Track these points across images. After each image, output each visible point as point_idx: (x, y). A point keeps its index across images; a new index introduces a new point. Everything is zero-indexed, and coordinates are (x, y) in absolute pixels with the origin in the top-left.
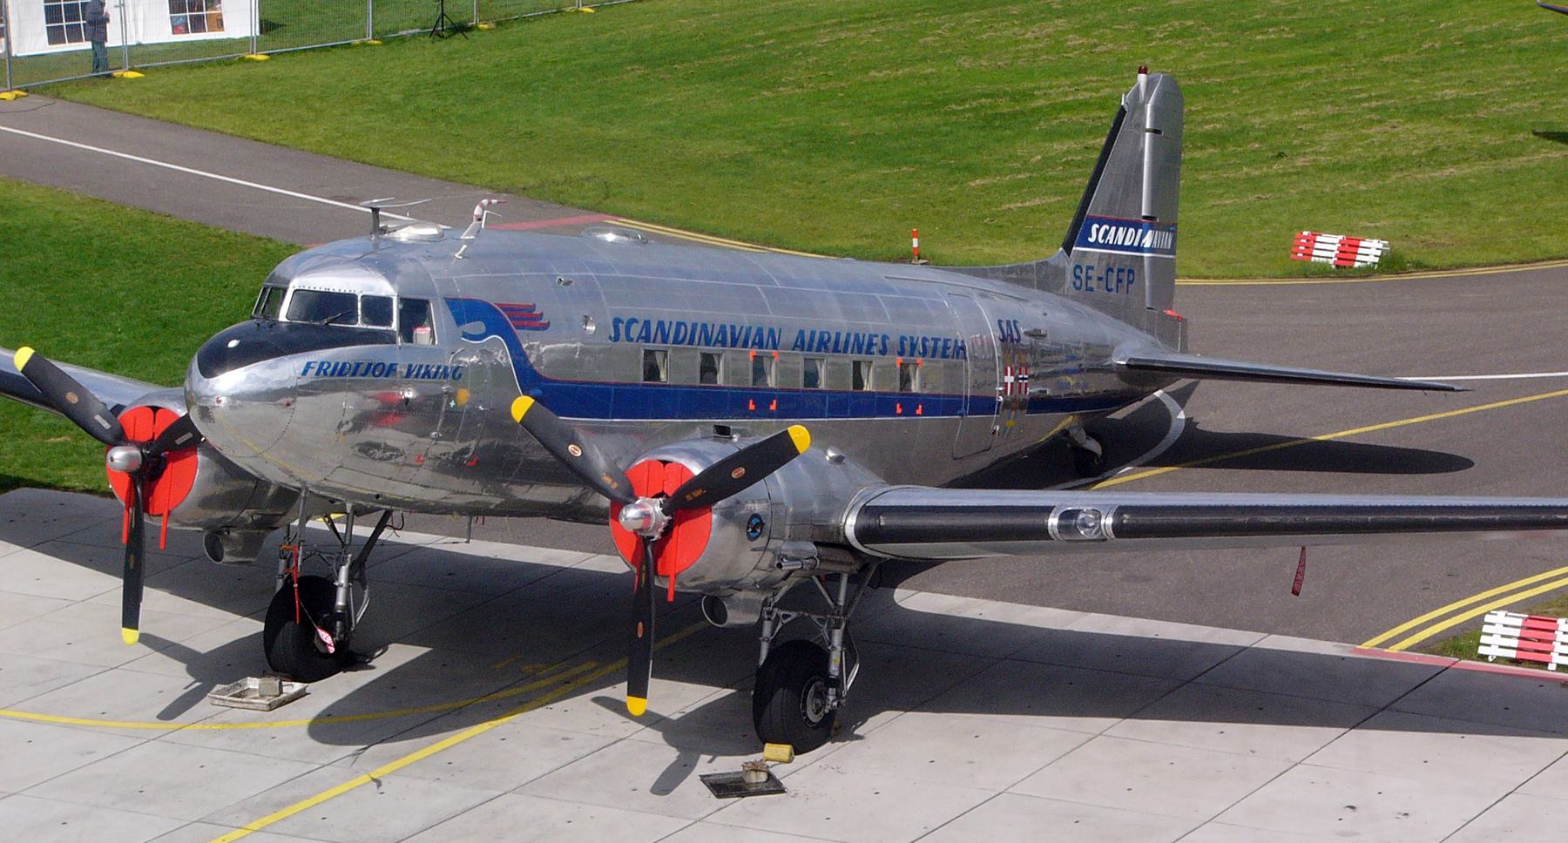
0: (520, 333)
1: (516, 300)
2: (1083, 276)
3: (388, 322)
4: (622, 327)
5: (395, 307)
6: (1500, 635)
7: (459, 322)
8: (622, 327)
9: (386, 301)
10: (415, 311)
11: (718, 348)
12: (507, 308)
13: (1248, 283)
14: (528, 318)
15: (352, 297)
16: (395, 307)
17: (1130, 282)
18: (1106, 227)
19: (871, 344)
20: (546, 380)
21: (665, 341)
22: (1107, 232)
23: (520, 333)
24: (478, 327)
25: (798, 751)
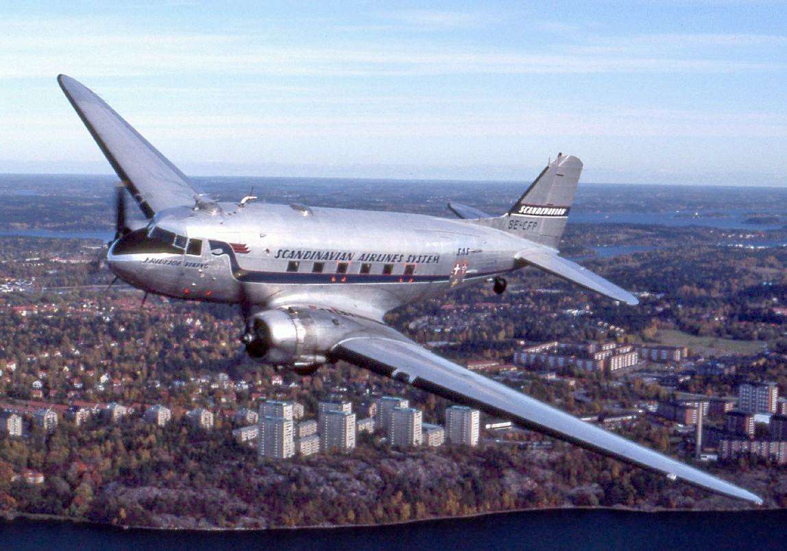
0: (237, 255)
1: (237, 242)
2: (514, 224)
3: (184, 247)
4: (281, 253)
5: (188, 242)
6: (621, 351)
8: (281, 253)
11: (324, 260)
12: (231, 244)
13: (46, 517)
14: (241, 249)
15: (185, 239)
16: (188, 242)
17: (534, 226)
18: (528, 207)
19: (395, 258)
20: (244, 270)
21: (299, 258)
22: (528, 209)
23: (237, 255)
24: (220, 251)
25: (559, 255)
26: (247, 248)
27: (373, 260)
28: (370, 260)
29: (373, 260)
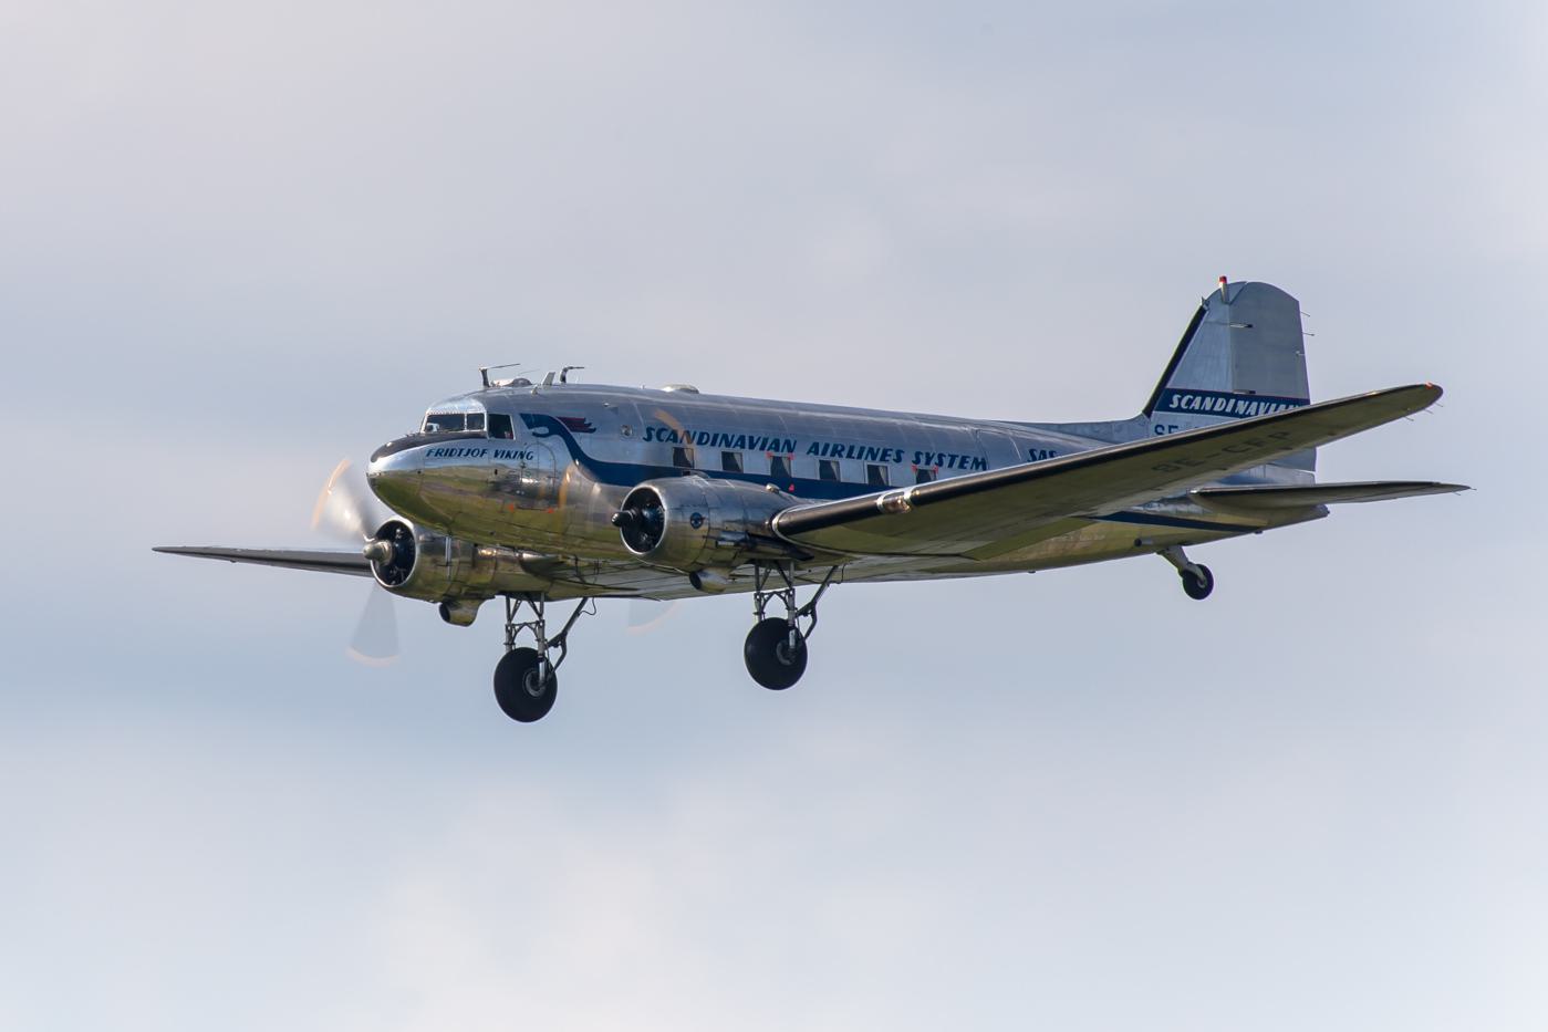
7: (469, 415)
9: (482, 415)
10: (499, 425)
24: (543, 430)
26: (590, 424)
27: (840, 456)
28: (833, 455)
29: (840, 456)
